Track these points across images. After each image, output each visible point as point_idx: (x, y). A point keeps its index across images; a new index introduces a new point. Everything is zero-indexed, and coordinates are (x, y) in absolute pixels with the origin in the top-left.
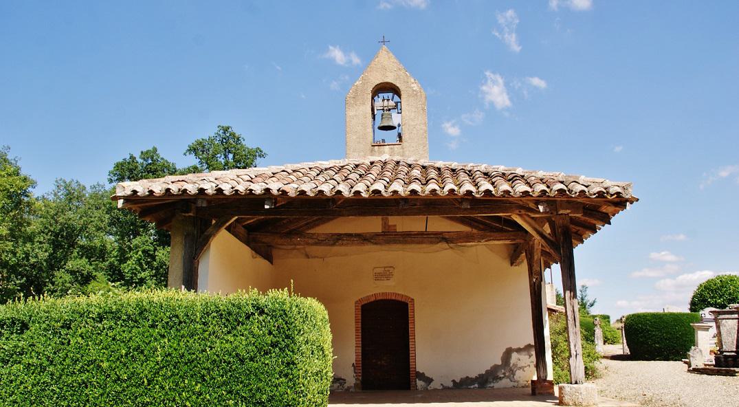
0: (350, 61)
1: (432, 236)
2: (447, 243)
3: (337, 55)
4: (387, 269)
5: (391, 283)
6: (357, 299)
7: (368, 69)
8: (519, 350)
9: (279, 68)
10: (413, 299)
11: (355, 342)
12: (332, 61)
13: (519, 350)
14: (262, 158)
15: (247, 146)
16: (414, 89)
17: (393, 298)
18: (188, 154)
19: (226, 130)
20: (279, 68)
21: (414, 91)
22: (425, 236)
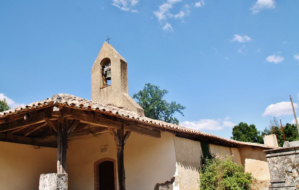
0: (246, 40)
1: (87, 131)
2: (92, 133)
3: (239, 38)
4: (105, 146)
5: (107, 153)
6: (95, 162)
7: (99, 54)
8: (162, 185)
9: (215, 49)
10: (115, 160)
11: (94, 182)
12: (237, 42)
13: (162, 185)
14: (167, 94)
15: (161, 90)
16: (115, 57)
17: (108, 160)
18: (133, 98)
19: (149, 85)
20: (215, 49)
21: (115, 58)
22: (84, 131)
